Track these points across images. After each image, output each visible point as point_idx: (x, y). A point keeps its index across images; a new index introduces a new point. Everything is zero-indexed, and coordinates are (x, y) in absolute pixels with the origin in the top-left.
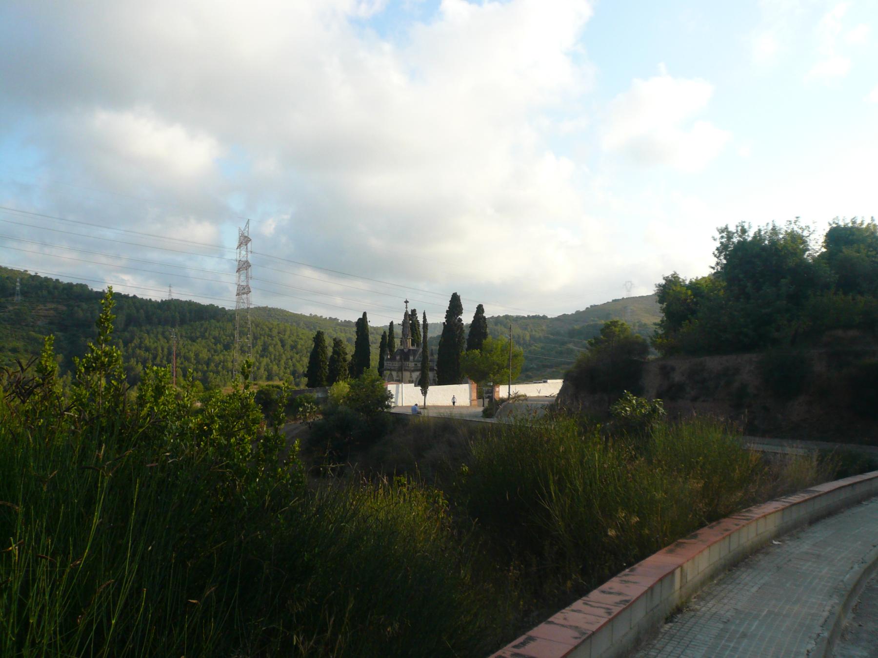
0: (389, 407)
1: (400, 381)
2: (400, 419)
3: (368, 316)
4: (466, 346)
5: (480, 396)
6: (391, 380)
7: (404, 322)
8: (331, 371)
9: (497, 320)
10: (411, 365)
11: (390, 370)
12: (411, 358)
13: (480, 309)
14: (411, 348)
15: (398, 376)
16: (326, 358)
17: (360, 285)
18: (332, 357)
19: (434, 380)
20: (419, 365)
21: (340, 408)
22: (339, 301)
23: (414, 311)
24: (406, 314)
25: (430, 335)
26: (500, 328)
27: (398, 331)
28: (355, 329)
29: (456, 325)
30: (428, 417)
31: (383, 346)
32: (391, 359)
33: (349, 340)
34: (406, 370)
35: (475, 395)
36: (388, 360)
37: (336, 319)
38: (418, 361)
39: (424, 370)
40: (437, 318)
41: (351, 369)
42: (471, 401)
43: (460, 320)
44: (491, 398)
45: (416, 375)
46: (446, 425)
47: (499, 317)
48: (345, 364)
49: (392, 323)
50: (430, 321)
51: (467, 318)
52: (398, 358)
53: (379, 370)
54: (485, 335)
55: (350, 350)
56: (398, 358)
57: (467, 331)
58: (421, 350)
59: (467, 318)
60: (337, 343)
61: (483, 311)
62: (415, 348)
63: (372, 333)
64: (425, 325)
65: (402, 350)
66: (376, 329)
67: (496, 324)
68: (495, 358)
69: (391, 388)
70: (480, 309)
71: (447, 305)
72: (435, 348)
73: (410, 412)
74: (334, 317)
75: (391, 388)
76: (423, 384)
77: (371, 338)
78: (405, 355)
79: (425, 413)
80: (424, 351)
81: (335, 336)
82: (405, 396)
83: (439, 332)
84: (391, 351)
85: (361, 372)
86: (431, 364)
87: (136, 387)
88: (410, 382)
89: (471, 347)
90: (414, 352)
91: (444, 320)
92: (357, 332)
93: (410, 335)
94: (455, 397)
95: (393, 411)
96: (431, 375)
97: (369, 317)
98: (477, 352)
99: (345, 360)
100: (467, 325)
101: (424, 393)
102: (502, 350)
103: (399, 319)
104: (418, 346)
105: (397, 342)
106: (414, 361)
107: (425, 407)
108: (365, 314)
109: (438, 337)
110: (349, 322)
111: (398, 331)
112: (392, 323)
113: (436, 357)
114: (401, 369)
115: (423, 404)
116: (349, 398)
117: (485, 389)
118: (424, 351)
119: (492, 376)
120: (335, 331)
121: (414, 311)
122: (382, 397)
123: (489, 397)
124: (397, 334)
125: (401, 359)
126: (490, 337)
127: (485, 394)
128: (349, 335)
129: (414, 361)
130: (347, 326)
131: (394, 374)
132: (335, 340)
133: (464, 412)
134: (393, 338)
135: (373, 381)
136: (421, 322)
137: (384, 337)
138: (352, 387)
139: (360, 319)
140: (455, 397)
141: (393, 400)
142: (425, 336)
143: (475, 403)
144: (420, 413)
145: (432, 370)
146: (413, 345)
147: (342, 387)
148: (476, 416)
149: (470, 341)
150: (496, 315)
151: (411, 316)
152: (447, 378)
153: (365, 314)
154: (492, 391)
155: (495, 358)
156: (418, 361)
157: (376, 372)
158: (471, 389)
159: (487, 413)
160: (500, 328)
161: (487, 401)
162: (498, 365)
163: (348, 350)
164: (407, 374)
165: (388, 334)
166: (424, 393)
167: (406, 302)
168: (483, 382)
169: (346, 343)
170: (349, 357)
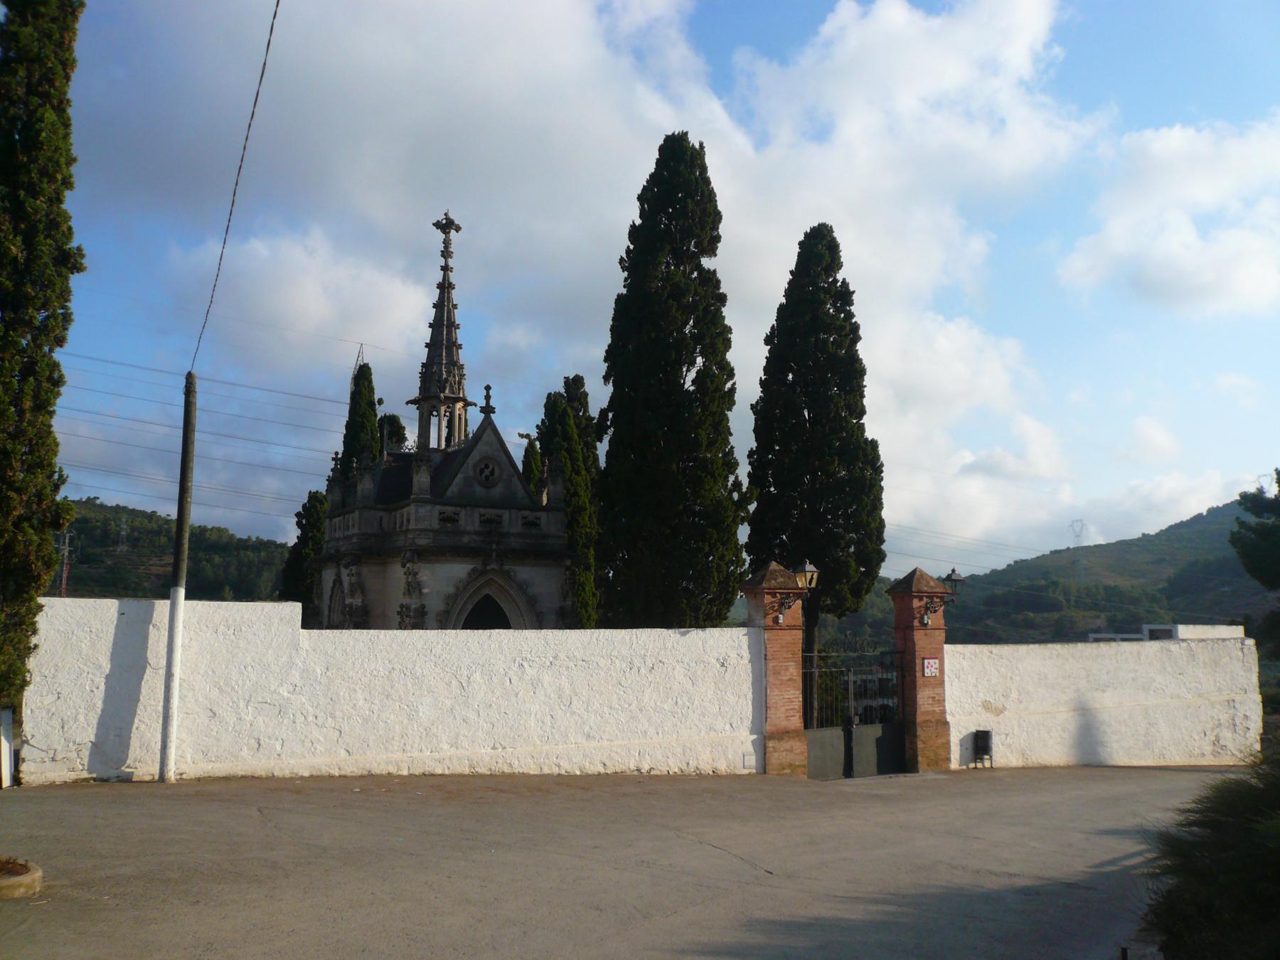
42: (766, 738)
61: (834, 261)
70: (819, 250)
108: (407, 403)
123: (884, 716)
158: (761, 660)
167: (446, 226)
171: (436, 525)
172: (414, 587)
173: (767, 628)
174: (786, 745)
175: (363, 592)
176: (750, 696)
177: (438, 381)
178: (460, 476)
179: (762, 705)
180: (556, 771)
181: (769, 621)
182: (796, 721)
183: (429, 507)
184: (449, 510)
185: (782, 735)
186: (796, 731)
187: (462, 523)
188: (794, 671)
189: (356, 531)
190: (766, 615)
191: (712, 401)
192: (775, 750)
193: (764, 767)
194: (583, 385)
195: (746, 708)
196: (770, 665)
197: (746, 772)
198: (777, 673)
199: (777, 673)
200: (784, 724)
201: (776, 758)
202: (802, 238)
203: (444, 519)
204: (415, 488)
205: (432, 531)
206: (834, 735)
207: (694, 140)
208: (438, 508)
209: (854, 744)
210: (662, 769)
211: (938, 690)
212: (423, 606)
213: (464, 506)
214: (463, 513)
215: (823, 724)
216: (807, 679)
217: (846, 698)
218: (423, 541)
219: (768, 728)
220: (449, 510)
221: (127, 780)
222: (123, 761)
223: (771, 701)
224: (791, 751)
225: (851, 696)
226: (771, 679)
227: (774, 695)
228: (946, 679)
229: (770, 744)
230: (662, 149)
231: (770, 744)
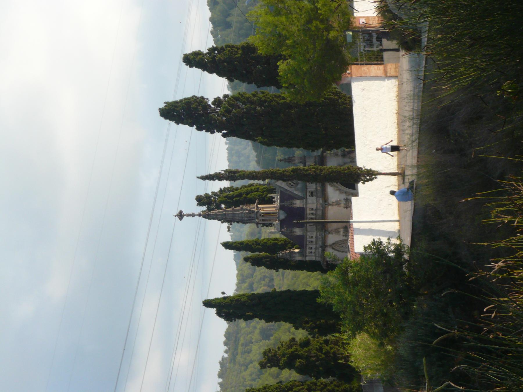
0: (398, 250)
1: (346, 227)
2: (424, 224)
3: (212, 296)
4: (272, 90)
5: (377, 58)
6: (344, 245)
7: (223, 219)
8: (327, 373)
9: (219, 23)
10: (312, 204)
11: (324, 247)
12: (298, 203)
13: (193, 60)
14: (277, 204)
15: (337, 231)
16: (302, 383)
17: (148, 311)
18: (300, 370)
19: (344, 156)
20: (312, 187)
21: (402, 351)
22: (183, 358)
23: (201, 200)
24: (207, 216)
25: (253, 166)
26: (234, 18)
27: (245, 232)
28: (242, 323)
29: (228, 111)
30: (418, 167)
31: (275, 264)
32: (302, 246)
33: (265, 335)
34: (324, 215)
35: (375, 69)
36: (301, 253)
37: (222, 364)
38: (305, 189)
39: (324, 178)
40: (217, 151)
41: (325, 330)
42: (387, 76)
43: (217, 101)
44: (381, 36)
45: (333, 193)
46: (437, 129)
47: (212, 20)
48: (315, 343)
49: (227, 245)
50: (222, 165)
51: (215, 87)
52: (298, 231)
53: (324, 271)
54: (249, 49)
55: (285, 332)
56: (298, 231)
57: (244, 88)
58: (280, 183)
59: (215, 87)
60: (270, 360)
61: (197, 54)
62: (277, 197)
63: (251, 286)
64: (230, 175)
65: (282, 223)
66: (242, 279)
67: (228, 25)
68: (294, 28)
69: (360, 244)
70: (193, 60)
71: (187, 131)
72: (279, 153)
73: (409, 205)
74: (218, 368)
75: (360, 244)
76: (352, 178)
77: (260, 289)
78: (293, 216)
79: (411, 174)
80: (282, 177)
81: (258, 366)
82: (376, 215)
83: (246, 147)
84: (284, 246)
85: (327, 309)
86: (310, 163)
87: (339, 283)
88: (348, 205)
89: (271, 78)
90: (285, 197)
91: (218, 135)
92: (247, 318)
93: (249, 207)
94: (379, 107)
95: (407, 241)
96: (333, 162)
97: (215, 294)
98: (282, 66)
99: (306, 344)
100: (232, 88)
101: (370, 175)
102: (278, 13)
103: (220, 231)
104: (272, 191)
105: (271, 233)
106: (303, 198)
107: (401, 174)
108: (208, 304)
109: (255, 149)
110: (228, 335)
111: (245, 232)
112: (227, 245)
113: (298, 152)
114: (323, 226)
115: (394, 179)
116: (383, 335)
117: (361, 46)
118: (282, 177)
119: (333, 34)
120: (246, 366)
121: (201, 200)
122: (378, 263)
123: (379, 39)
124: (252, 234)
125: (301, 226)
126: (253, 40)
127: (371, 48)
128: (256, 335)
129: (303, 198)
130: (237, 340)
131: (332, 239)
132: (263, 366)
133: (408, 88)
134: (257, 243)
135: (346, 282)
136: (225, 184)
137: (256, 262)
138: (358, 328)
139: (219, 314)
140: (379, 107)
141: (384, 240)
142: (252, 176)
143: (391, 68)
144: (411, 183)
145: (322, 160)
146: (270, 201)
147: (361, 350)
148: (415, 68)
149: (262, 82)
150: (210, 26)
151: (211, 207)
152: (336, 126)
153: (208, 304)
154: (368, 34)
155: (294, 28)
156: (305, 189)
157: (332, 277)
158: (362, 78)
159: (410, 44)
160: (234, 18)
161: (386, 43)
162: (309, 21)
163: (286, 338)
164: (333, 213)
165: (249, 254)
166: (370, 175)
167: (181, 216)
168: (347, 55)
169: (272, 340)
170: (301, 334)
171: (314, 198)
172: (338, 203)
173: (352, 76)
174: (389, 70)
175: (339, 228)
176: (373, 81)
177: (250, 213)
178: (295, 192)
179: (376, 78)
180: (396, 135)
181: (349, 76)
182: (381, 67)
183: (308, 200)
184: (308, 194)
185: (385, 71)
186: (384, 67)
187: (312, 190)
188: (365, 68)
189: (315, 233)
190: (347, 77)
191: (269, 98)
192: (390, 73)
193: (396, 77)
194: (201, 196)
195: (377, 83)
196: (363, 75)
197: (397, 82)
198: (366, 73)
199: (366, 73)
200: (382, 71)
201: (393, 73)
202: (188, 66)
203: (312, 194)
204: (301, 206)
205: (317, 198)
206: (386, 55)
207: (162, 106)
208: (308, 197)
209: (388, 48)
210: (396, 107)
211: (370, 18)
212: (344, 199)
213: (307, 189)
214: (309, 190)
215: (382, 60)
216: (366, 64)
217: (373, 51)
218: (321, 201)
219: (383, 76)
220: (308, 194)
221: (399, 231)
222: (395, 232)
223: (375, 75)
224: (390, 69)
225: (372, 49)
226: (368, 75)
227: (372, 74)
228: (366, 16)
229: (388, 75)
230: (166, 118)
231: (388, 75)
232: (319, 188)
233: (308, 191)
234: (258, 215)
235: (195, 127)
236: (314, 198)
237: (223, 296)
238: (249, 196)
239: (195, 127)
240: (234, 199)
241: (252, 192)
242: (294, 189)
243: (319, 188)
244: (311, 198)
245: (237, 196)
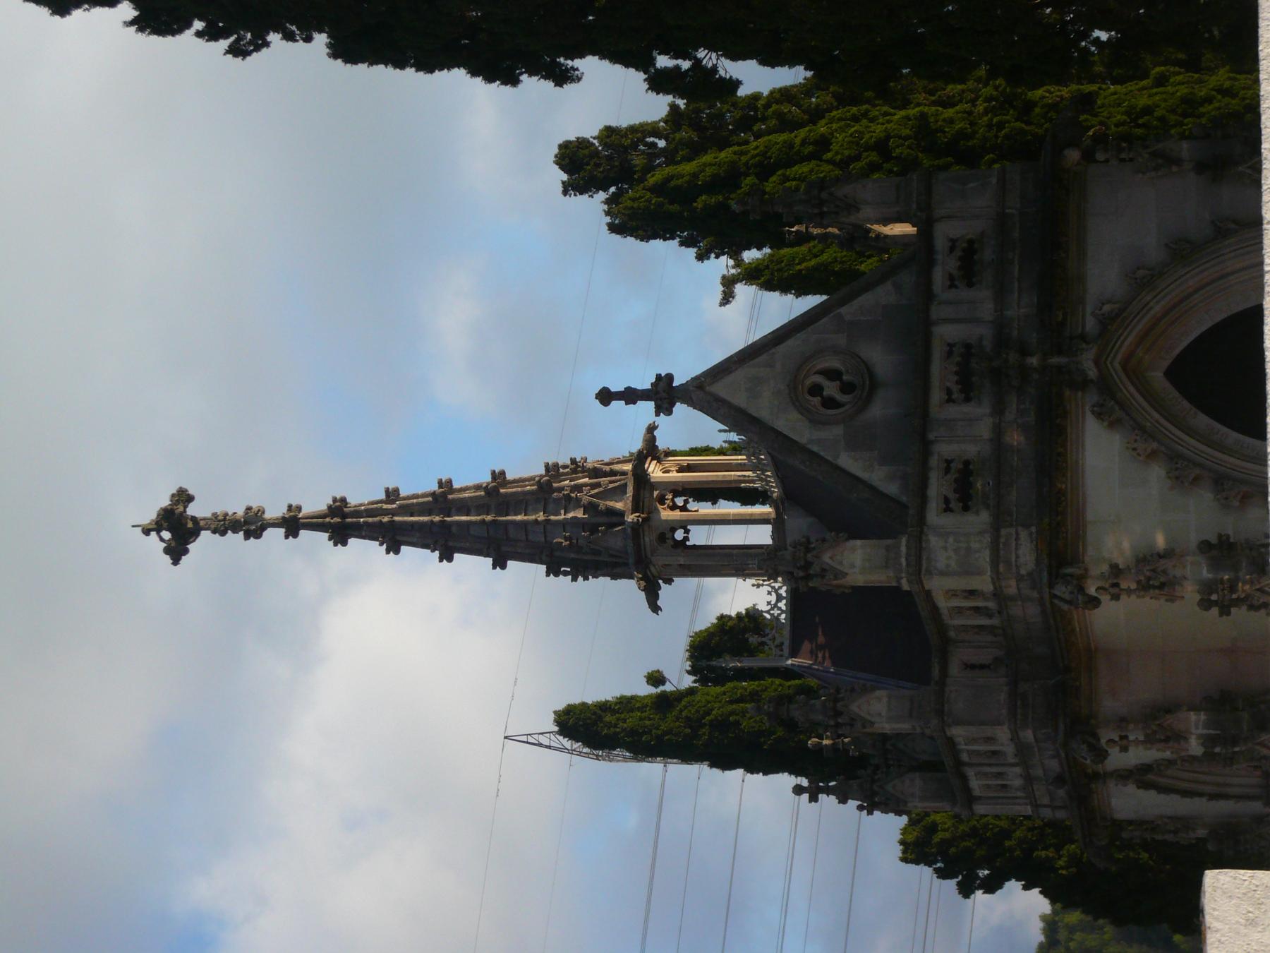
108: (655, 608)
167: (177, 528)
171: (980, 519)
177: (593, 529)
178: (846, 461)
183: (934, 541)
184: (938, 487)
187: (971, 450)
194: (582, 143)
203: (963, 498)
204: (880, 578)
205: (996, 528)
208: (934, 516)
212: (1205, 547)
213: (926, 447)
214: (944, 449)
218: (1025, 554)
220: (938, 487)
232: (1015, 438)
233: (934, 461)
234: (649, 539)
235: (321, 39)
236: (980, 519)
237: (652, 690)
238: (771, 184)
239: (321, 39)
240: (699, 204)
241: (790, 164)
242: (837, 431)
243: (1015, 438)
244: (947, 521)
245: (713, 186)
